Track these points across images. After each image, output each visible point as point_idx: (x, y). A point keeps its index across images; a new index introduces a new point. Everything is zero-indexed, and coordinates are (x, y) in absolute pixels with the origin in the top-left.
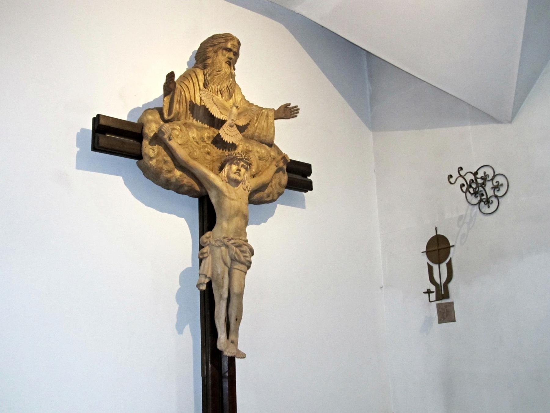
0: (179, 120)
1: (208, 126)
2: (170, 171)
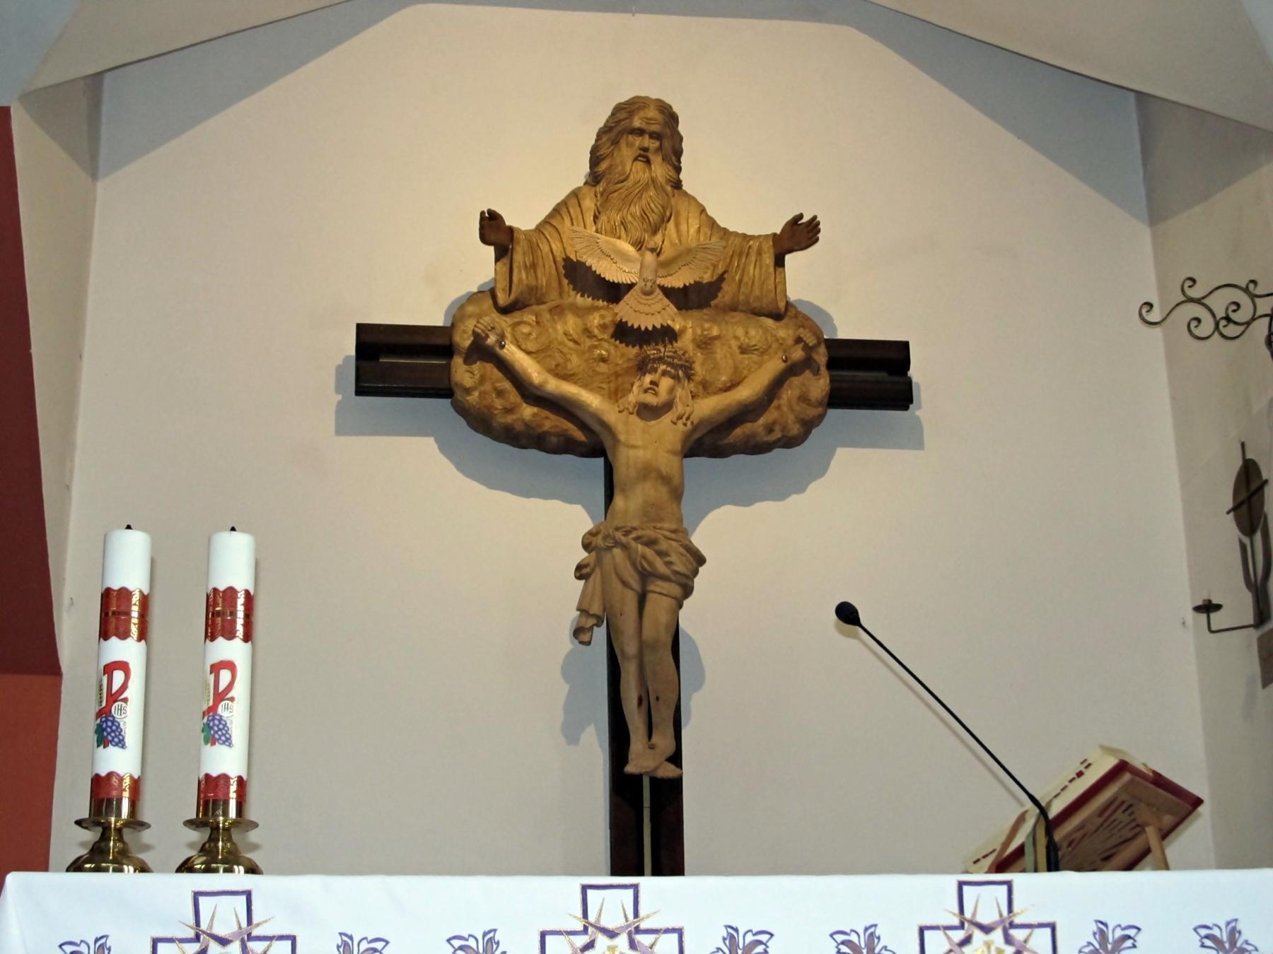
0: (544, 303)
1: (605, 303)
2: (509, 411)
